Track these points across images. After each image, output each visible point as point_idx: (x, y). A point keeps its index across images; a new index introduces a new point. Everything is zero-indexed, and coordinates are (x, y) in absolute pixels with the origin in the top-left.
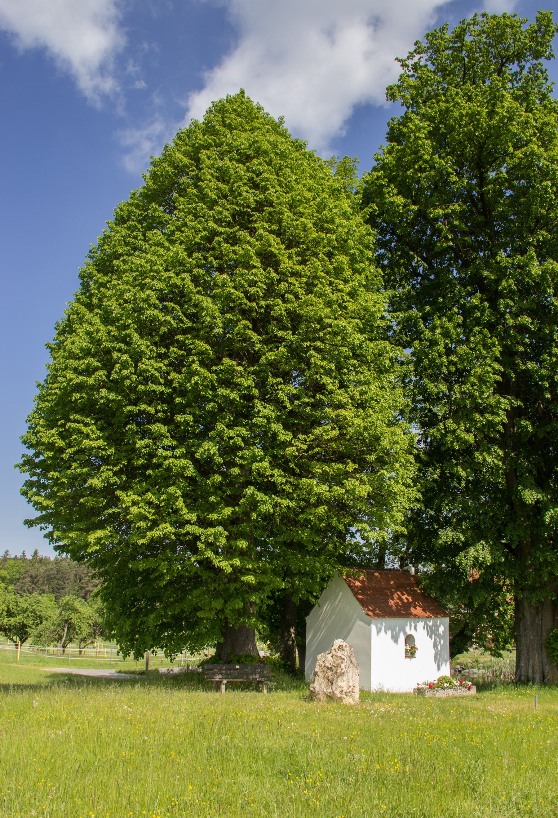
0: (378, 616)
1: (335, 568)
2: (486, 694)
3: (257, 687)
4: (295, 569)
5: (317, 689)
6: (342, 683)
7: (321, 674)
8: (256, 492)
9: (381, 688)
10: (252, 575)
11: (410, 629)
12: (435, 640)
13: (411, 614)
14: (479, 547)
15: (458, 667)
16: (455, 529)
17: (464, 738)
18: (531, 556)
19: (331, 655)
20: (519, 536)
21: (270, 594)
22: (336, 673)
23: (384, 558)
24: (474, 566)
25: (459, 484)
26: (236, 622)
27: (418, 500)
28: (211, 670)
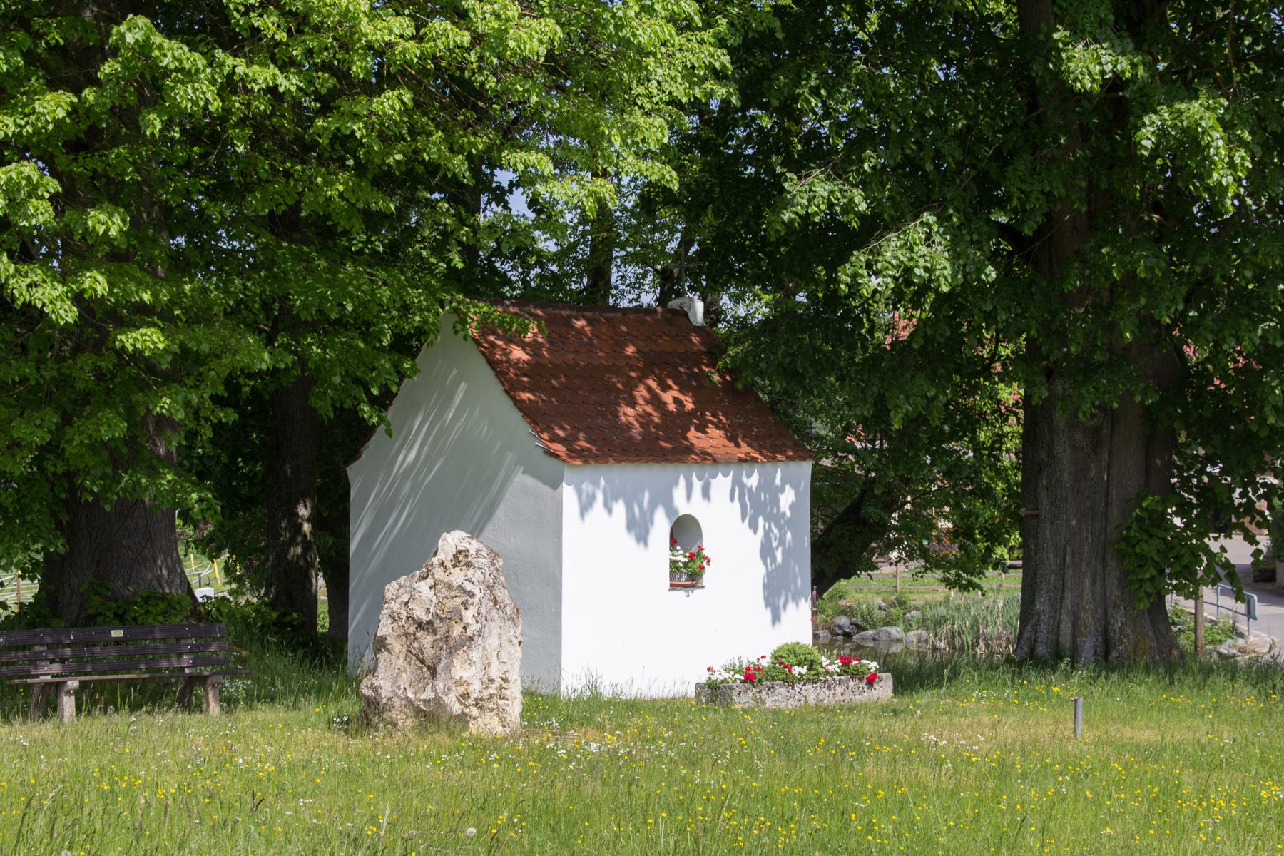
0: (584, 457)
1: (442, 303)
2: (925, 698)
3: (187, 695)
4: (305, 307)
5: (385, 693)
6: (466, 671)
7: (397, 645)
8: (157, 39)
9: (593, 688)
10: (155, 325)
11: (689, 497)
12: (767, 533)
13: (690, 449)
14: (916, 232)
15: (844, 621)
16: (839, 174)
17: (846, 824)
18: (1084, 262)
19: (430, 581)
20: (1048, 195)
21: (221, 390)
22: (447, 638)
23: (608, 273)
24: (897, 298)
25: (860, 22)
26: (105, 490)
27: (719, 75)
28: (24, 648)
